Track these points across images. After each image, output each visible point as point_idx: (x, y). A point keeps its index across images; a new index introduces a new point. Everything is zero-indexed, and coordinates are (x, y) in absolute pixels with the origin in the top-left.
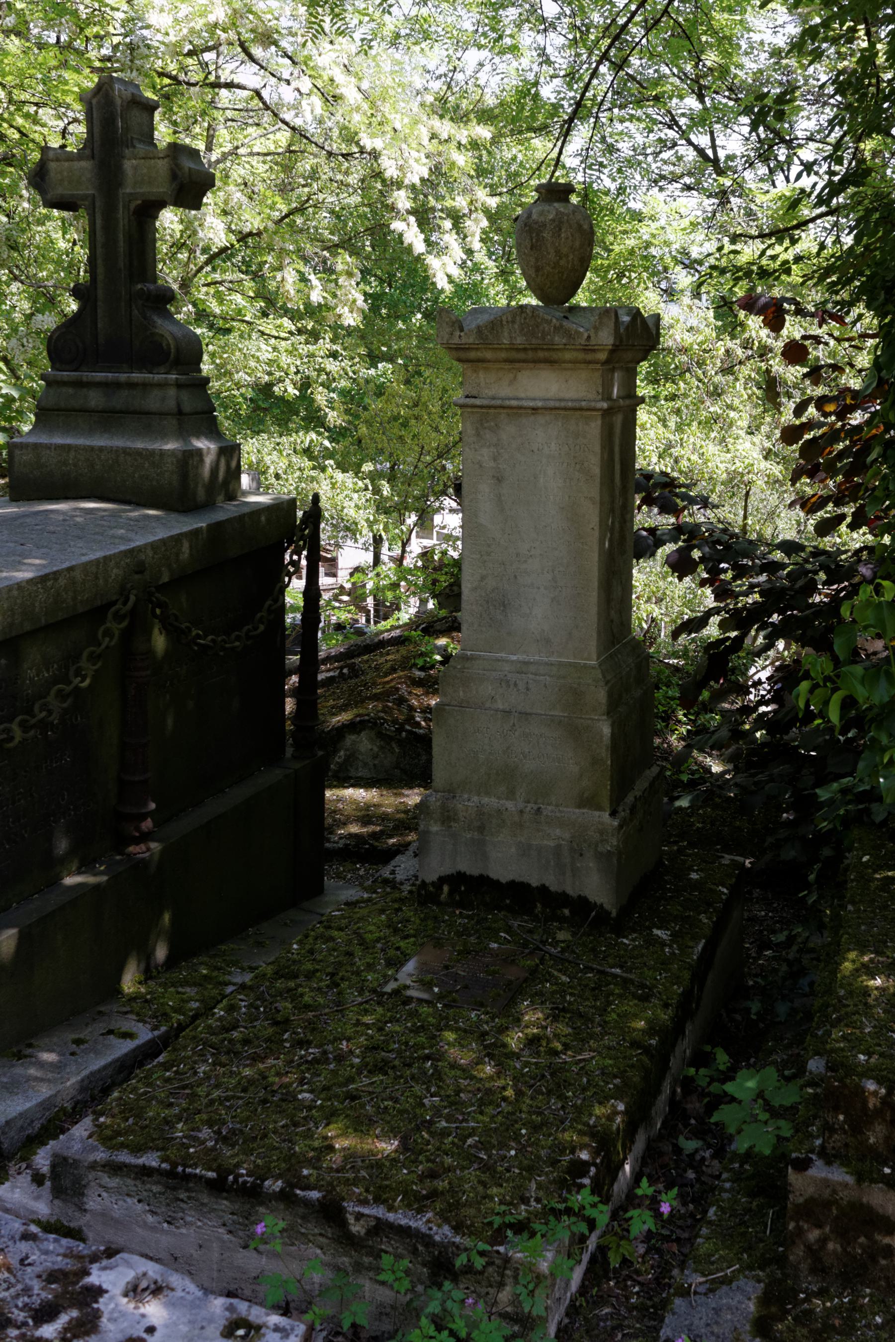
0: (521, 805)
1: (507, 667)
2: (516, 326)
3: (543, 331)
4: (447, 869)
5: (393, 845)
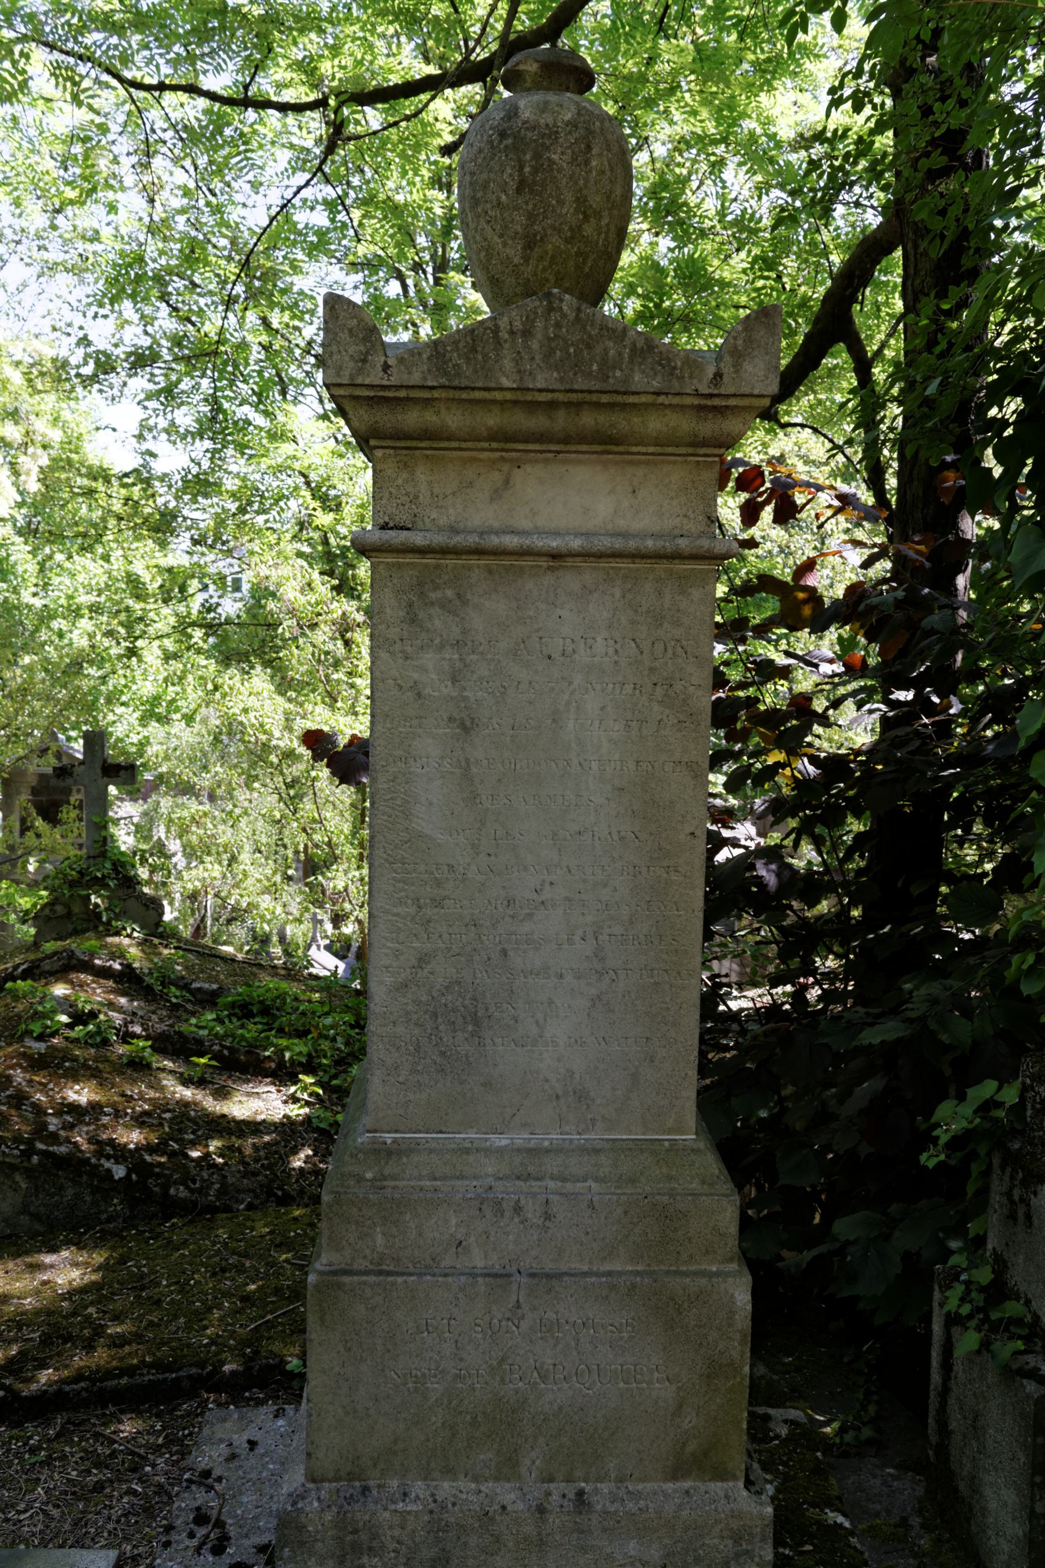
1: (490, 1167)
2: (535, 345)
3: (604, 361)
5: (50, 1383)
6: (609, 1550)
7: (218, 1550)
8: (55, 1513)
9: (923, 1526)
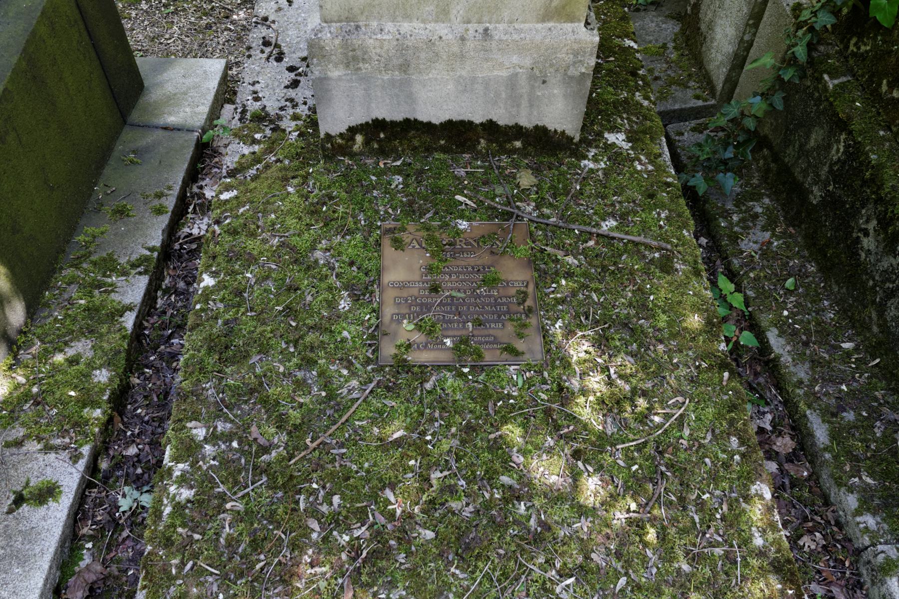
0: (460, 28)
4: (360, 117)
6: (501, 61)
7: (279, 59)
8: (187, 39)
9: (674, 48)
